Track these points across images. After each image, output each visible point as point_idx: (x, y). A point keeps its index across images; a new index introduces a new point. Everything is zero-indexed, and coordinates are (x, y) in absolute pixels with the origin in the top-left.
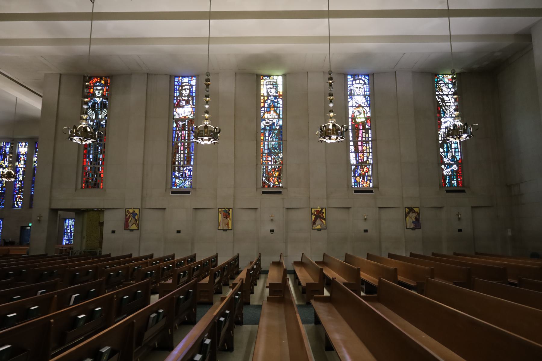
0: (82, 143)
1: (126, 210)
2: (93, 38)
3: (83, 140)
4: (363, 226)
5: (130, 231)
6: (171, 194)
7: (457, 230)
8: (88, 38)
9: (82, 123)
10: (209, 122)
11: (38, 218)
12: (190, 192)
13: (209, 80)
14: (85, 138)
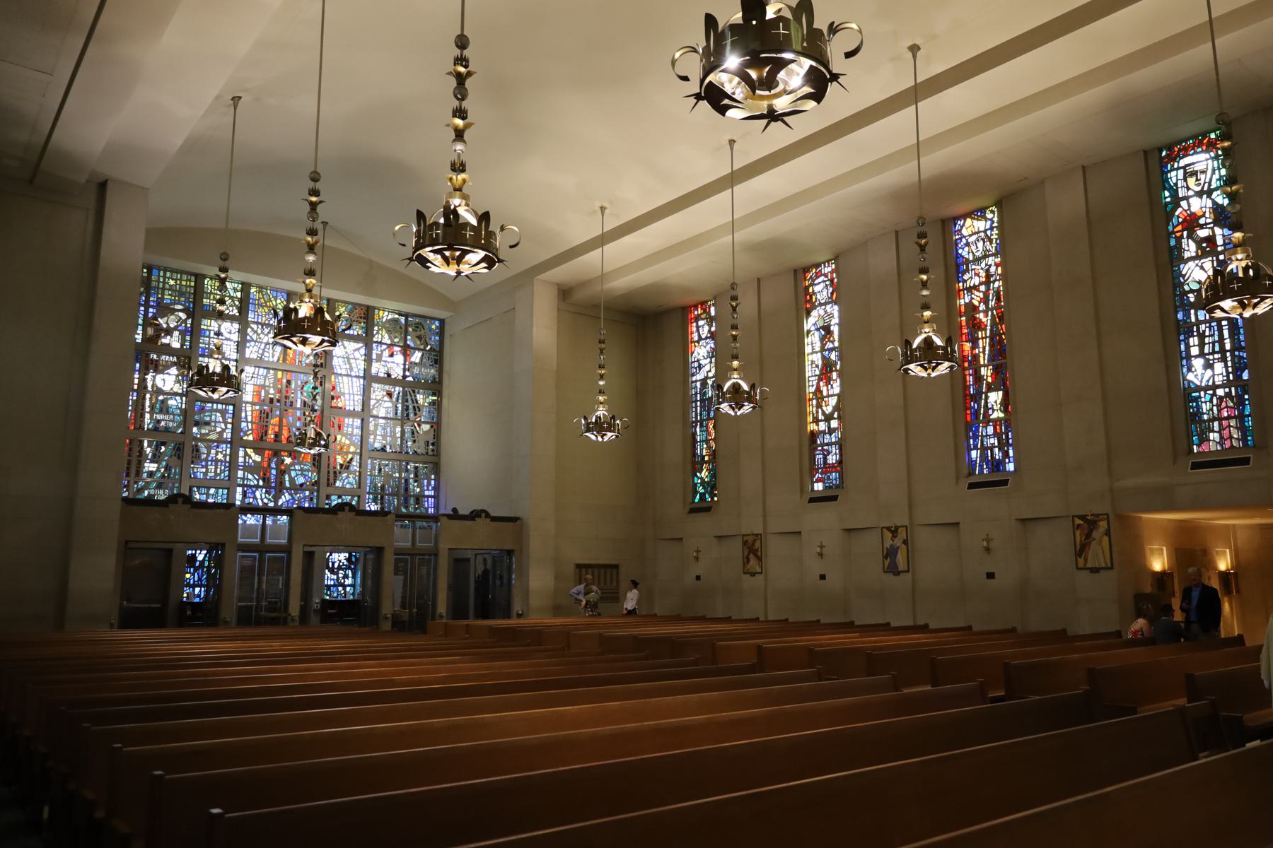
0: (736, 413)
1: (1104, 514)
2: (1219, 18)
3: (930, 368)
4: (817, 568)
5: (751, 576)
6: (1191, 469)
7: (985, 576)
8: (914, 145)
9: (1233, 258)
10: (739, 374)
11: (985, 544)
12: (1250, 457)
13: (926, 234)
14: (930, 362)
